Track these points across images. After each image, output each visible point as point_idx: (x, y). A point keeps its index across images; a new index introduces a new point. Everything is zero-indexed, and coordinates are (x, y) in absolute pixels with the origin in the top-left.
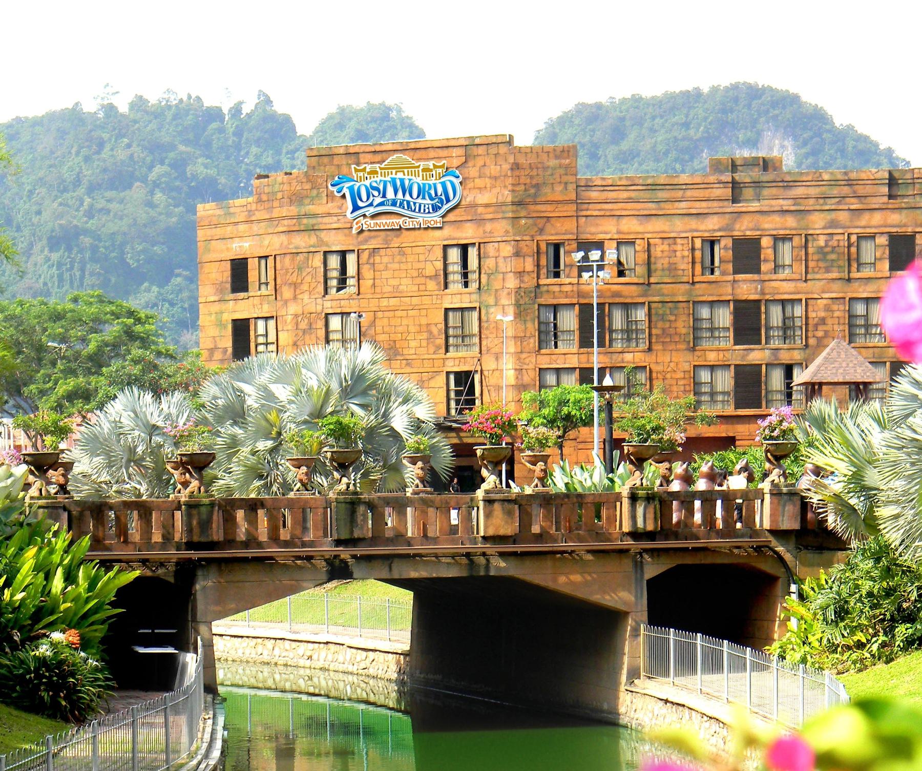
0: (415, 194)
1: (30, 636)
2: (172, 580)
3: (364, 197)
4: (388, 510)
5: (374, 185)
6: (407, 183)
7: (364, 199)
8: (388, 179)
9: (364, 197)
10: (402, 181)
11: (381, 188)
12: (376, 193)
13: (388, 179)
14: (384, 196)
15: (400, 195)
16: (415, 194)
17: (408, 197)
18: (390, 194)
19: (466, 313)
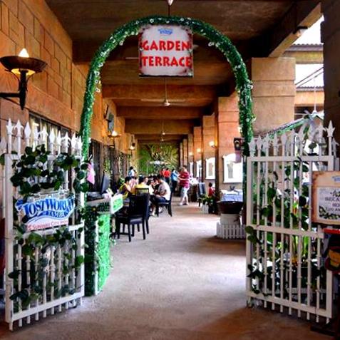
0: (57, 208)
1: (30, 271)
2: (319, 269)
3: (33, 211)
4: (33, 224)
5: (38, 204)
6: (53, 201)
7: (33, 212)
8: (44, 200)
9: (33, 211)
10: (51, 200)
11: (41, 205)
12: (38, 208)
13: (44, 200)
14: (43, 210)
15: (50, 209)
16: (57, 208)
17: (54, 210)
18: (45, 209)
19: (18, 100)
